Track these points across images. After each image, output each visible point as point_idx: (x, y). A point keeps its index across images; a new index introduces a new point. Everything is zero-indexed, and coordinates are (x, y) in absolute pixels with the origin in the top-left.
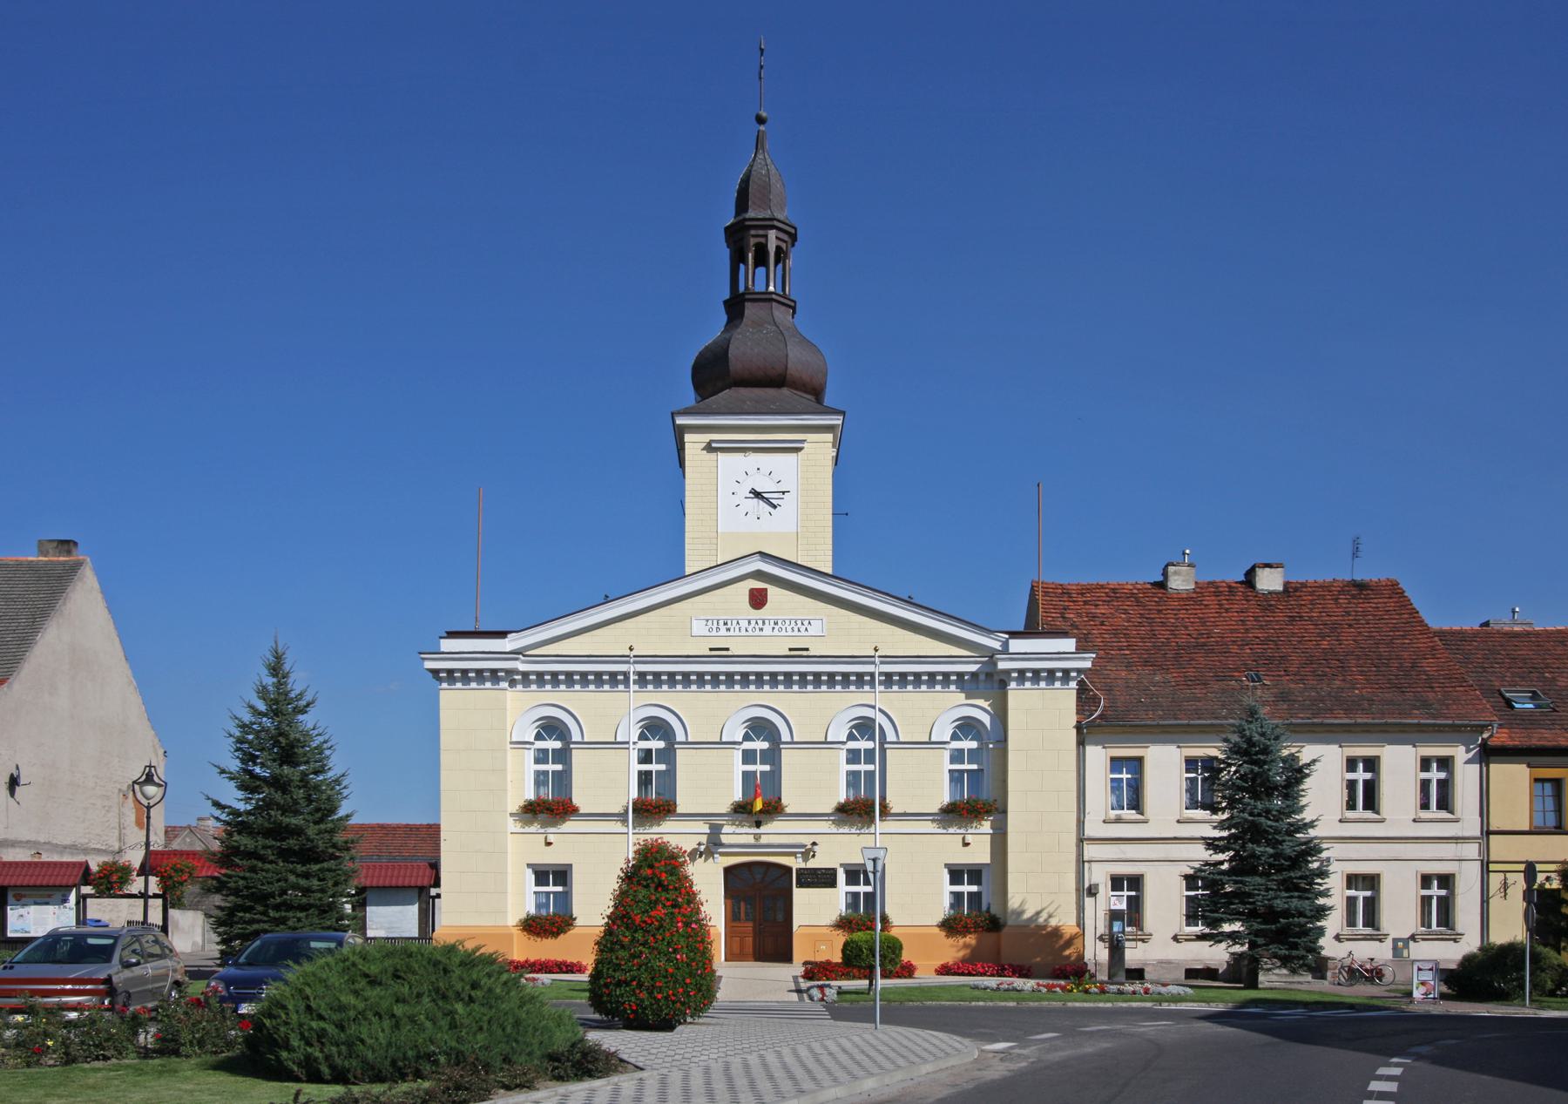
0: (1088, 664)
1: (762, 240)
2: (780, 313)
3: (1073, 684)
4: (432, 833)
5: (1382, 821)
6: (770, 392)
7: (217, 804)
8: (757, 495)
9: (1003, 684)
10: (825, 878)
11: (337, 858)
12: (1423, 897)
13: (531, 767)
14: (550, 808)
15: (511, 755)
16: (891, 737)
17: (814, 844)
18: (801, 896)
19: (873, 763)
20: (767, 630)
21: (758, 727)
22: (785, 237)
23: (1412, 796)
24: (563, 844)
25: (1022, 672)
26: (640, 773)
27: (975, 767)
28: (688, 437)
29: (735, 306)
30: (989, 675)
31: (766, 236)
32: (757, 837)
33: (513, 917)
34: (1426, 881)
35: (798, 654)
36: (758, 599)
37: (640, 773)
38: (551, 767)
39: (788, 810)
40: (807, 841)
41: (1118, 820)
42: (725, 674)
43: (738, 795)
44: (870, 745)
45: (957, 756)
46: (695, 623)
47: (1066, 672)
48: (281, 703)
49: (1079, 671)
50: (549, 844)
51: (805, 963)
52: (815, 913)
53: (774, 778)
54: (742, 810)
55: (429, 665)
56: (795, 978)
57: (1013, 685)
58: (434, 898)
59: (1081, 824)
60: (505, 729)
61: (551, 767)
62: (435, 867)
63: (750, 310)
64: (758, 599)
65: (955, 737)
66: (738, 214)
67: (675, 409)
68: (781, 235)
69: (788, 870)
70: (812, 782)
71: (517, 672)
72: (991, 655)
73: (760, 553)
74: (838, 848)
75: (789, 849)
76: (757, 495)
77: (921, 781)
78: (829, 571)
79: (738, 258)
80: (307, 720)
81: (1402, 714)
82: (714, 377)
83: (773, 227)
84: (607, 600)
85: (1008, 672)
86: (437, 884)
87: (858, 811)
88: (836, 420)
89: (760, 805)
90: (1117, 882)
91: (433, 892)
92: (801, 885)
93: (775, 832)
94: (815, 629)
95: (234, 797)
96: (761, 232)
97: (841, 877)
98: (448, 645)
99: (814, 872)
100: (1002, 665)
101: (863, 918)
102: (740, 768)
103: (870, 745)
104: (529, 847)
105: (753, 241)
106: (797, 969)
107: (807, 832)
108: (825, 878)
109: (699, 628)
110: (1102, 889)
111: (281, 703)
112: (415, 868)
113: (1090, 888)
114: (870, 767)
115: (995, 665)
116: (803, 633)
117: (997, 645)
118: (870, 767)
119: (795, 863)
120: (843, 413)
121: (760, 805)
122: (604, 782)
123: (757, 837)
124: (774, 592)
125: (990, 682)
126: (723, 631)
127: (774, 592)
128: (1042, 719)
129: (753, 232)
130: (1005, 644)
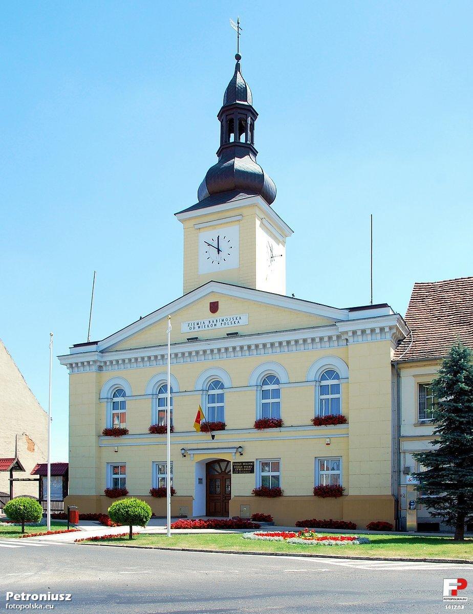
10: (247, 468)
18: (235, 478)
20: (218, 324)
52: (242, 486)
54: (262, 424)
64: (214, 307)
74: (259, 447)
97: (257, 467)
99: (242, 464)
108: (247, 468)
119: (233, 458)
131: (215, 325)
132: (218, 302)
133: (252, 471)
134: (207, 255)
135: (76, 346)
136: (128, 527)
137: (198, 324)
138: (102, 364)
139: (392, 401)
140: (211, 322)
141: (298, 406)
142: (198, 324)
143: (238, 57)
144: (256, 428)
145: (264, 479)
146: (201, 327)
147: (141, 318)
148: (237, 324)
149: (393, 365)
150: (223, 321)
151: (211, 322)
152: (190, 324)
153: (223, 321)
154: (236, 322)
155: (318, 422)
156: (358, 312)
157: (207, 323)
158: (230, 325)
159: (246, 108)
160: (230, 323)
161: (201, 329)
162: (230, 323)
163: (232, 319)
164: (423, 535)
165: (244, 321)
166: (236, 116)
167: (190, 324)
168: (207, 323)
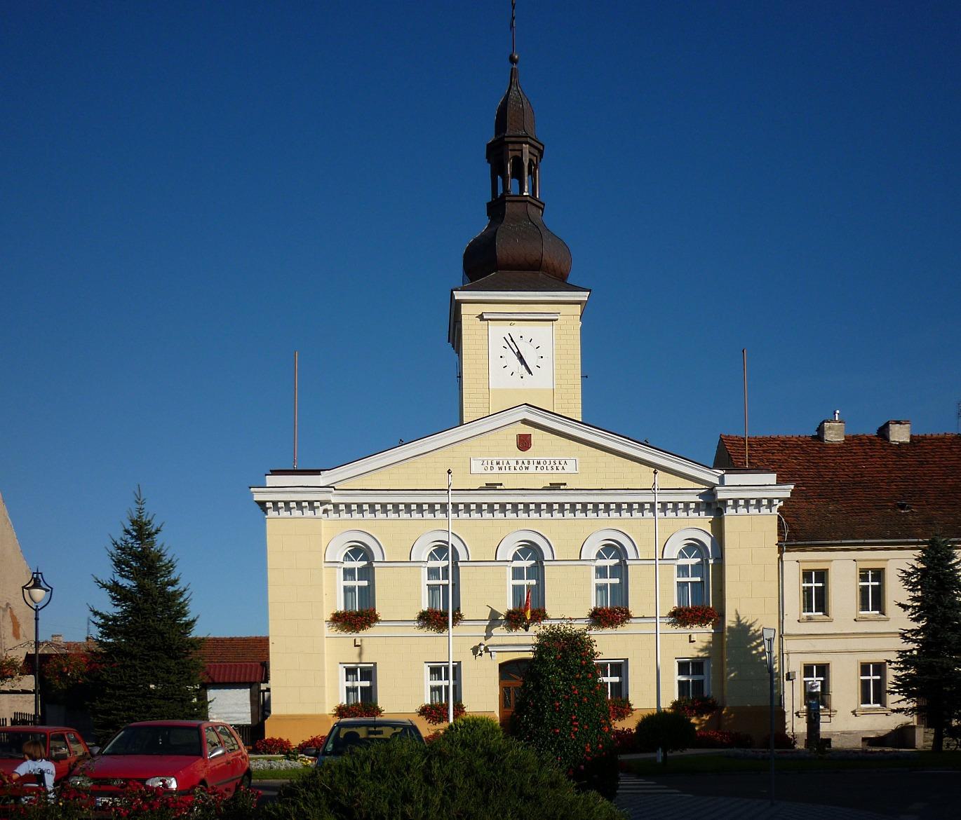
1: (518, 153)
2: (532, 211)
3: (775, 510)
4: (267, 639)
5: (888, 620)
6: (529, 274)
7: (96, 613)
11: (191, 660)
12: (863, 681)
13: (341, 583)
14: (356, 618)
15: (325, 572)
16: (462, 557)
19: (447, 578)
20: (532, 468)
22: (536, 153)
23: (853, 598)
24: (453, 644)
26: (514, 586)
27: (698, 579)
28: (465, 309)
29: (496, 209)
33: (414, 707)
34: (865, 669)
36: (524, 443)
37: (514, 586)
38: (357, 583)
39: (466, 617)
41: (809, 619)
42: (490, 502)
44: (445, 563)
45: (683, 570)
47: (770, 501)
48: (141, 530)
53: (538, 591)
55: (258, 497)
58: (264, 691)
59: (781, 623)
60: (321, 552)
61: (357, 583)
62: (265, 666)
63: (509, 208)
64: (524, 443)
65: (682, 555)
66: (497, 133)
67: (452, 288)
68: (533, 150)
71: (328, 502)
73: (526, 404)
78: (581, 420)
79: (498, 169)
80: (159, 540)
81: (865, 539)
82: (487, 265)
83: (526, 143)
84: (402, 443)
85: (724, 502)
86: (266, 680)
88: (583, 296)
90: (808, 670)
91: (263, 687)
94: (570, 468)
95: (110, 608)
96: (517, 147)
98: (272, 480)
100: (720, 496)
103: (445, 563)
104: (339, 648)
105: (511, 154)
110: (797, 675)
111: (141, 530)
112: (248, 664)
113: (788, 674)
114: (446, 582)
115: (715, 495)
116: (560, 471)
117: (716, 481)
118: (446, 582)
120: (590, 291)
122: (400, 594)
125: (713, 505)
126: (496, 470)
128: (752, 536)
129: (511, 147)
130: (722, 478)
132: (703, 674)
137: (498, 463)
139: (241, 638)
140: (520, 462)
142: (498, 463)
146: (503, 468)
148: (560, 471)
149: (721, 439)
150: (539, 463)
151: (520, 462)
152: (486, 462)
153: (539, 463)
154: (560, 468)
155: (832, 561)
156: (290, 713)
157: (513, 464)
158: (550, 471)
160: (549, 468)
161: (503, 470)
162: (549, 468)
163: (552, 463)
164: (623, 673)
167: (486, 462)
168: (513, 464)
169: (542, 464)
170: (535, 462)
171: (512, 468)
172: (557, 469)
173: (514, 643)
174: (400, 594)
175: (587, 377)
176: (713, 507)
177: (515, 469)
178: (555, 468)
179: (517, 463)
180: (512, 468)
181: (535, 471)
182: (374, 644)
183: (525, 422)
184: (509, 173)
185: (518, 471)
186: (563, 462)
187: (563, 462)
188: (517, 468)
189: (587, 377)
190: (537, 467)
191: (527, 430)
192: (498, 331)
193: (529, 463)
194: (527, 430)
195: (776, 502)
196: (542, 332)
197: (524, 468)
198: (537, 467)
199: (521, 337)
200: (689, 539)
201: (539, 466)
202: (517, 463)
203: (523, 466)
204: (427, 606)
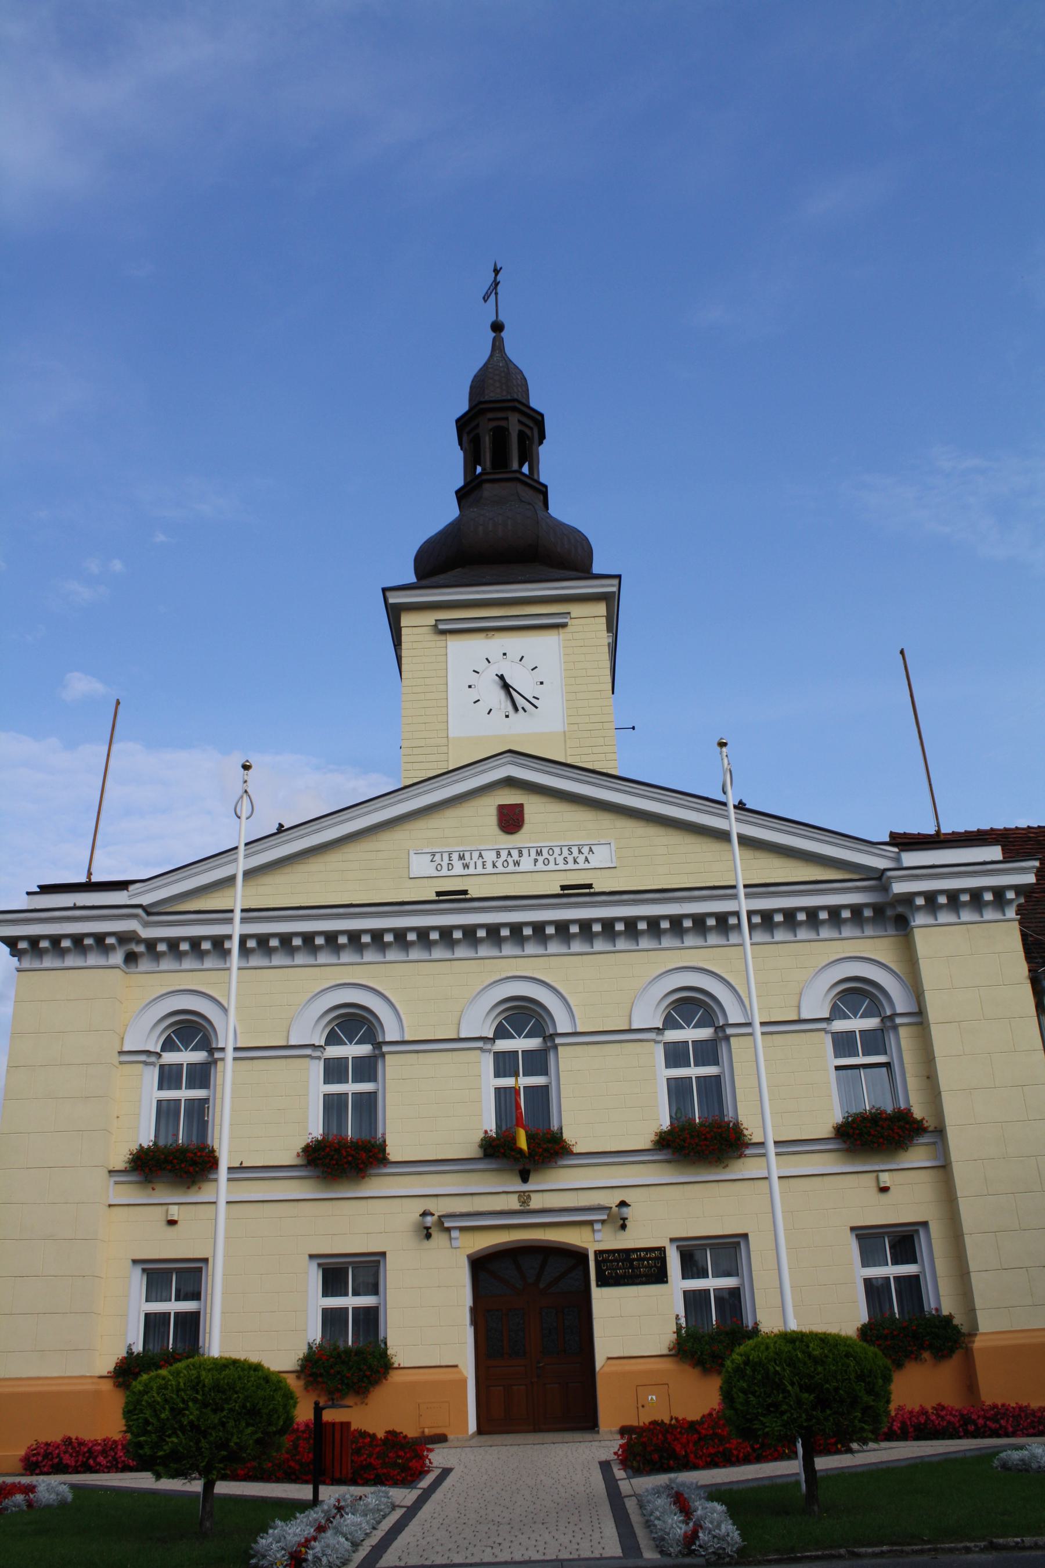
0: (1030, 879)
1: (503, 423)
8: (506, 687)
9: (902, 923)
10: (640, 1268)
17: (623, 1204)
18: (606, 1302)
20: (527, 864)
21: (522, 1015)
24: (367, 1219)
25: (930, 897)
26: (327, 1097)
28: (406, 620)
30: (879, 910)
31: (507, 419)
32: (524, 1197)
35: (576, 892)
36: (511, 820)
40: (611, 1199)
43: (489, 1123)
46: (414, 858)
47: (999, 893)
49: (1018, 889)
50: (884, 1190)
51: (624, 1431)
52: (632, 1327)
54: (496, 1150)
56: (605, 1466)
57: (920, 919)
64: (511, 820)
69: (577, 1257)
70: (612, 1101)
72: (879, 879)
73: (510, 751)
74: (668, 1210)
75: (584, 1217)
76: (506, 687)
77: (786, 1090)
83: (514, 409)
85: (908, 899)
87: (702, 1140)
89: (524, 1143)
92: (603, 1282)
93: (558, 1188)
94: (601, 857)
99: (626, 1255)
100: (899, 888)
101: (714, 1337)
102: (490, 1082)
106: (607, 1445)
107: (616, 1184)
108: (640, 1268)
109: (421, 865)
116: (582, 864)
119: (593, 1241)
121: (524, 1143)
122: (266, 1114)
123: (524, 1197)
124: (535, 809)
126: (458, 869)
127: (535, 809)
129: (490, 415)
131: (517, 863)
133: (659, 1276)
134: (539, 676)
135: (46, 889)
136: (626, 1500)
138: (141, 948)
141: (786, 1090)
143: (497, 327)
144: (660, 1150)
145: (695, 1301)
146: (472, 866)
147: (281, 829)
150: (539, 853)
153: (539, 853)
158: (562, 867)
159: (470, 415)
162: (560, 860)
165: (601, 857)
166: (499, 430)
169: (545, 854)
170: (533, 852)
171: (489, 865)
172: (575, 861)
173: (498, 1208)
174: (266, 1114)
175: (633, 728)
176: (889, 913)
177: (494, 866)
178: (570, 859)
179: (498, 855)
180: (489, 865)
181: (531, 868)
182: (210, 1224)
183: (510, 782)
184: (487, 439)
185: (501, 869)
186: (585, 850)
187: (585, 850)
188: (499, 864)
189: (633, 728)
190: (536, 861)
191: (510, 797)
192: (465, 652)
193: (521, 854)
194: (510, 797)
195: (1010, 895)
196: (543, 647)
197: (511, 864)
198: (536, 861)
199: (505, 654)
200: (488, 1013)
201: (540, 859)
202: (498, 855)
203: (510, 860)
204: (321, 1132)
